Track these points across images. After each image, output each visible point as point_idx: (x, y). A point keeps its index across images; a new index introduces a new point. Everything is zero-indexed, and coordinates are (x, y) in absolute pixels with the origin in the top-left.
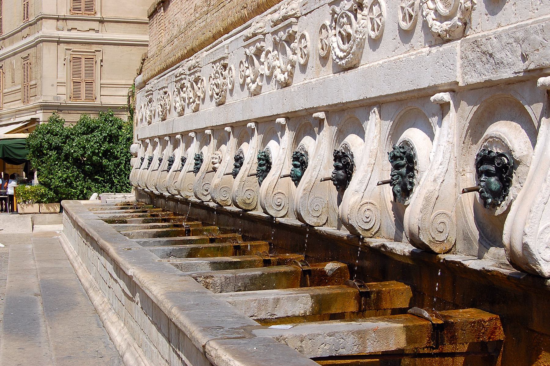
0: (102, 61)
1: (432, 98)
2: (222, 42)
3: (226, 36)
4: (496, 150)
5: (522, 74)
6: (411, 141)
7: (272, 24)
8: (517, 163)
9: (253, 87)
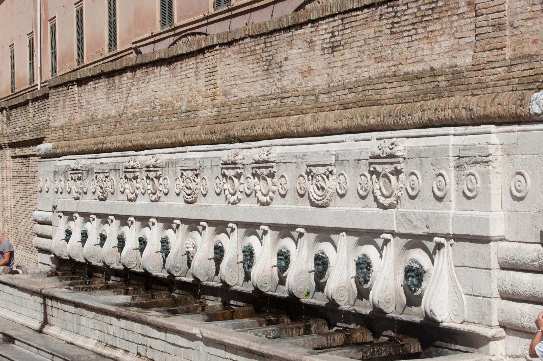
5: (426, 234)
8: (425, 272)
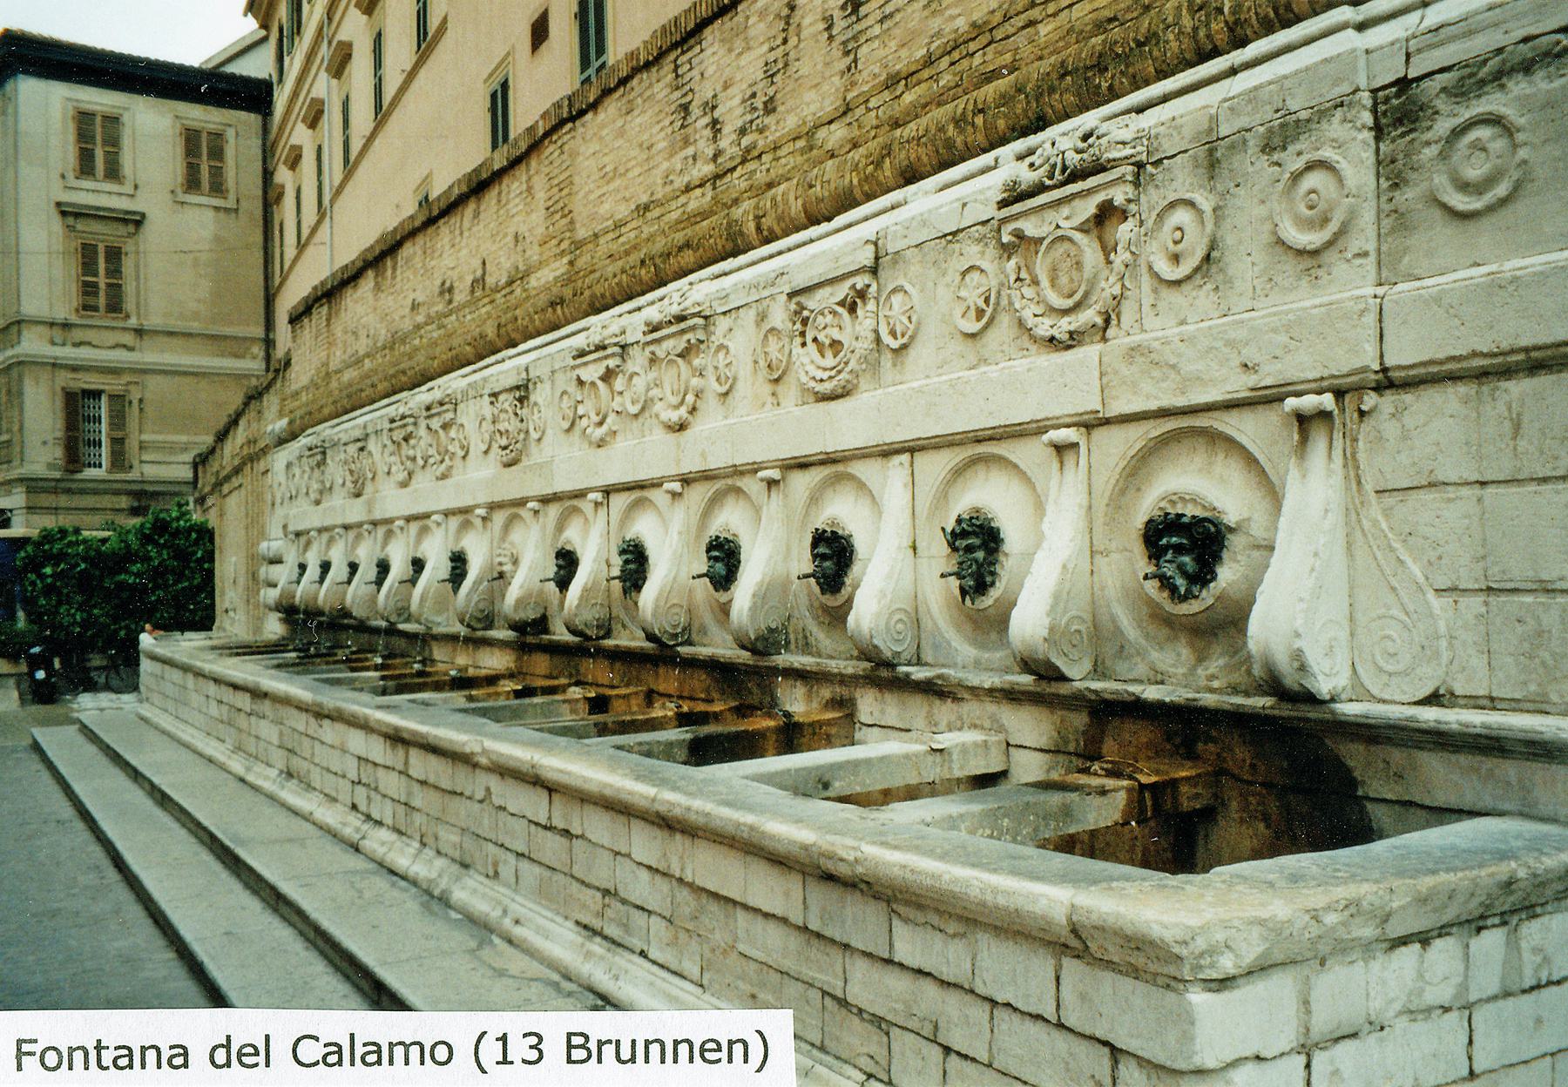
0: (141, 401)
3: (512, 351)
4: (1190, 511)
8: (1231, 530)
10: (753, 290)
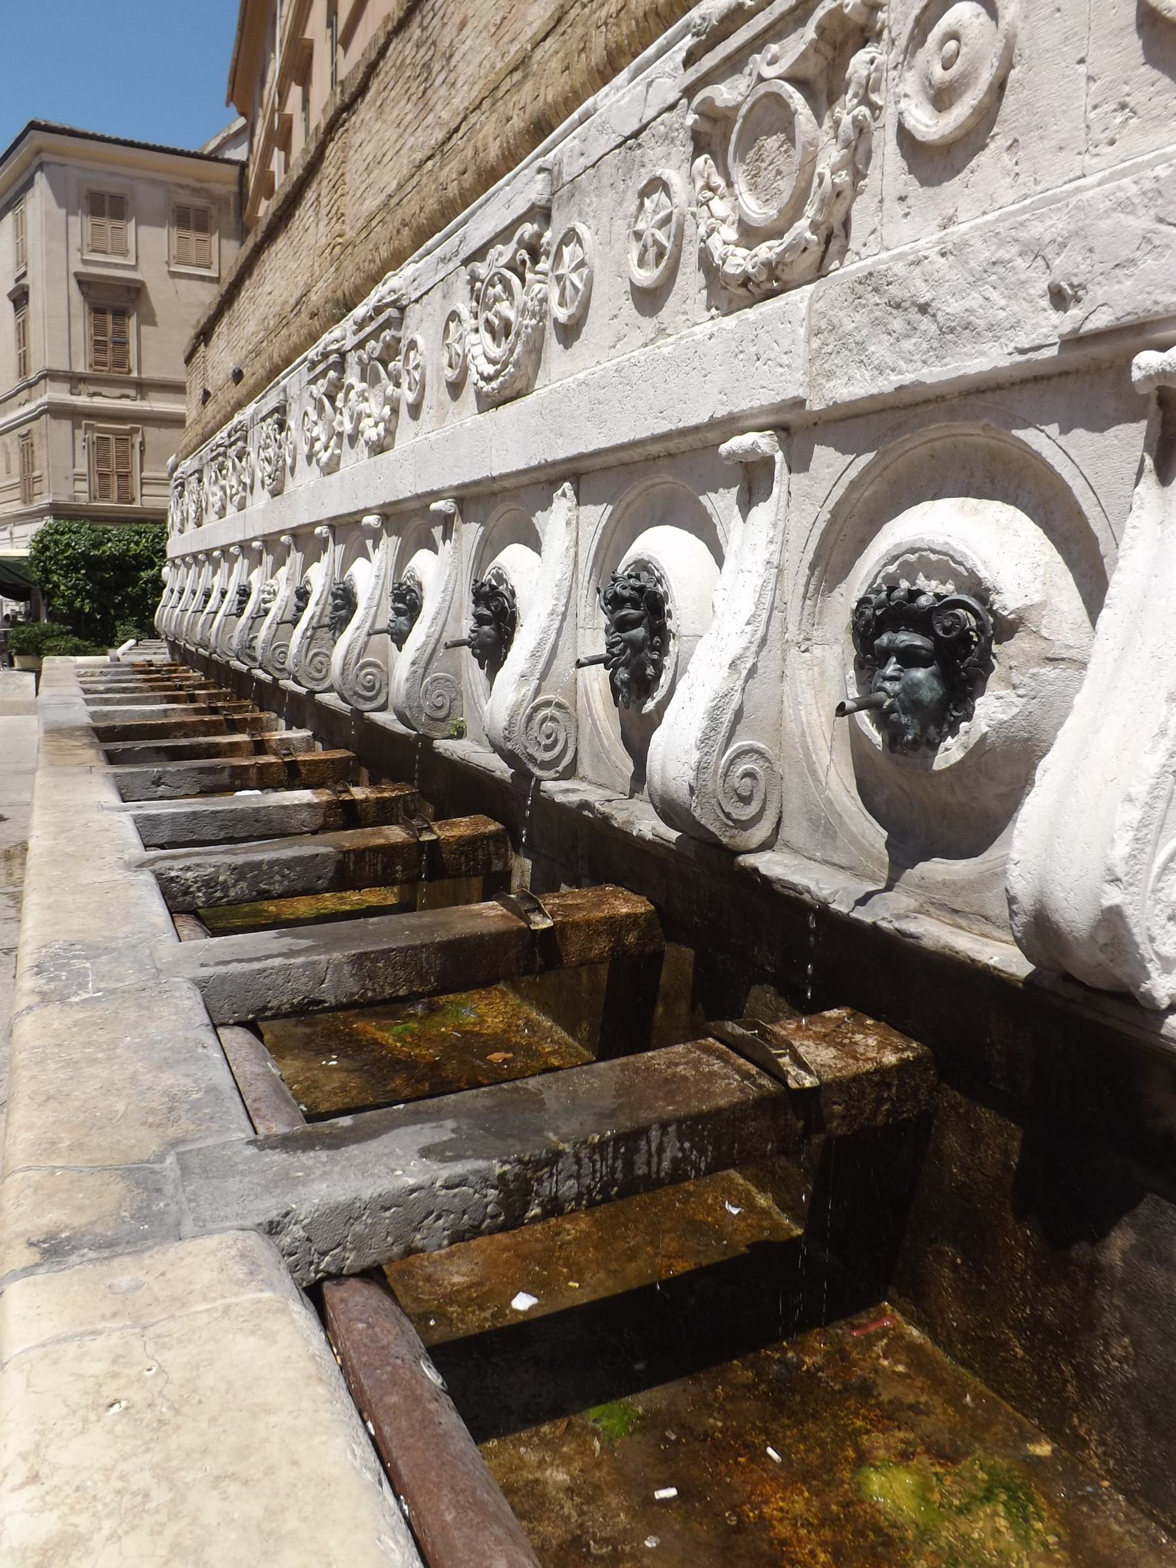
1: (724, 448)
2: (278, 383)
4: (931, 588)
5: (1053, 352)
6: (657, 562)
7: (355, 327)
8: (1006, 628)
9: (324, 457)
10: (441, 265)
